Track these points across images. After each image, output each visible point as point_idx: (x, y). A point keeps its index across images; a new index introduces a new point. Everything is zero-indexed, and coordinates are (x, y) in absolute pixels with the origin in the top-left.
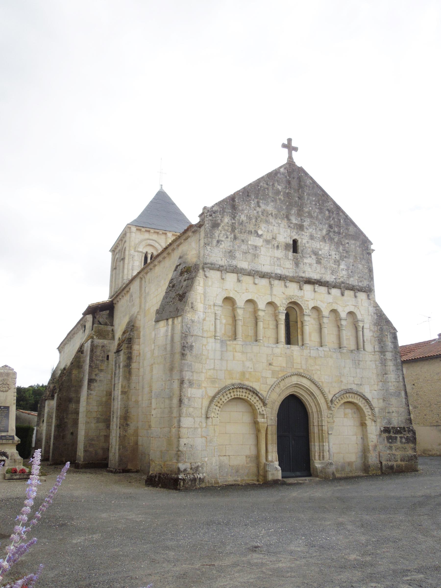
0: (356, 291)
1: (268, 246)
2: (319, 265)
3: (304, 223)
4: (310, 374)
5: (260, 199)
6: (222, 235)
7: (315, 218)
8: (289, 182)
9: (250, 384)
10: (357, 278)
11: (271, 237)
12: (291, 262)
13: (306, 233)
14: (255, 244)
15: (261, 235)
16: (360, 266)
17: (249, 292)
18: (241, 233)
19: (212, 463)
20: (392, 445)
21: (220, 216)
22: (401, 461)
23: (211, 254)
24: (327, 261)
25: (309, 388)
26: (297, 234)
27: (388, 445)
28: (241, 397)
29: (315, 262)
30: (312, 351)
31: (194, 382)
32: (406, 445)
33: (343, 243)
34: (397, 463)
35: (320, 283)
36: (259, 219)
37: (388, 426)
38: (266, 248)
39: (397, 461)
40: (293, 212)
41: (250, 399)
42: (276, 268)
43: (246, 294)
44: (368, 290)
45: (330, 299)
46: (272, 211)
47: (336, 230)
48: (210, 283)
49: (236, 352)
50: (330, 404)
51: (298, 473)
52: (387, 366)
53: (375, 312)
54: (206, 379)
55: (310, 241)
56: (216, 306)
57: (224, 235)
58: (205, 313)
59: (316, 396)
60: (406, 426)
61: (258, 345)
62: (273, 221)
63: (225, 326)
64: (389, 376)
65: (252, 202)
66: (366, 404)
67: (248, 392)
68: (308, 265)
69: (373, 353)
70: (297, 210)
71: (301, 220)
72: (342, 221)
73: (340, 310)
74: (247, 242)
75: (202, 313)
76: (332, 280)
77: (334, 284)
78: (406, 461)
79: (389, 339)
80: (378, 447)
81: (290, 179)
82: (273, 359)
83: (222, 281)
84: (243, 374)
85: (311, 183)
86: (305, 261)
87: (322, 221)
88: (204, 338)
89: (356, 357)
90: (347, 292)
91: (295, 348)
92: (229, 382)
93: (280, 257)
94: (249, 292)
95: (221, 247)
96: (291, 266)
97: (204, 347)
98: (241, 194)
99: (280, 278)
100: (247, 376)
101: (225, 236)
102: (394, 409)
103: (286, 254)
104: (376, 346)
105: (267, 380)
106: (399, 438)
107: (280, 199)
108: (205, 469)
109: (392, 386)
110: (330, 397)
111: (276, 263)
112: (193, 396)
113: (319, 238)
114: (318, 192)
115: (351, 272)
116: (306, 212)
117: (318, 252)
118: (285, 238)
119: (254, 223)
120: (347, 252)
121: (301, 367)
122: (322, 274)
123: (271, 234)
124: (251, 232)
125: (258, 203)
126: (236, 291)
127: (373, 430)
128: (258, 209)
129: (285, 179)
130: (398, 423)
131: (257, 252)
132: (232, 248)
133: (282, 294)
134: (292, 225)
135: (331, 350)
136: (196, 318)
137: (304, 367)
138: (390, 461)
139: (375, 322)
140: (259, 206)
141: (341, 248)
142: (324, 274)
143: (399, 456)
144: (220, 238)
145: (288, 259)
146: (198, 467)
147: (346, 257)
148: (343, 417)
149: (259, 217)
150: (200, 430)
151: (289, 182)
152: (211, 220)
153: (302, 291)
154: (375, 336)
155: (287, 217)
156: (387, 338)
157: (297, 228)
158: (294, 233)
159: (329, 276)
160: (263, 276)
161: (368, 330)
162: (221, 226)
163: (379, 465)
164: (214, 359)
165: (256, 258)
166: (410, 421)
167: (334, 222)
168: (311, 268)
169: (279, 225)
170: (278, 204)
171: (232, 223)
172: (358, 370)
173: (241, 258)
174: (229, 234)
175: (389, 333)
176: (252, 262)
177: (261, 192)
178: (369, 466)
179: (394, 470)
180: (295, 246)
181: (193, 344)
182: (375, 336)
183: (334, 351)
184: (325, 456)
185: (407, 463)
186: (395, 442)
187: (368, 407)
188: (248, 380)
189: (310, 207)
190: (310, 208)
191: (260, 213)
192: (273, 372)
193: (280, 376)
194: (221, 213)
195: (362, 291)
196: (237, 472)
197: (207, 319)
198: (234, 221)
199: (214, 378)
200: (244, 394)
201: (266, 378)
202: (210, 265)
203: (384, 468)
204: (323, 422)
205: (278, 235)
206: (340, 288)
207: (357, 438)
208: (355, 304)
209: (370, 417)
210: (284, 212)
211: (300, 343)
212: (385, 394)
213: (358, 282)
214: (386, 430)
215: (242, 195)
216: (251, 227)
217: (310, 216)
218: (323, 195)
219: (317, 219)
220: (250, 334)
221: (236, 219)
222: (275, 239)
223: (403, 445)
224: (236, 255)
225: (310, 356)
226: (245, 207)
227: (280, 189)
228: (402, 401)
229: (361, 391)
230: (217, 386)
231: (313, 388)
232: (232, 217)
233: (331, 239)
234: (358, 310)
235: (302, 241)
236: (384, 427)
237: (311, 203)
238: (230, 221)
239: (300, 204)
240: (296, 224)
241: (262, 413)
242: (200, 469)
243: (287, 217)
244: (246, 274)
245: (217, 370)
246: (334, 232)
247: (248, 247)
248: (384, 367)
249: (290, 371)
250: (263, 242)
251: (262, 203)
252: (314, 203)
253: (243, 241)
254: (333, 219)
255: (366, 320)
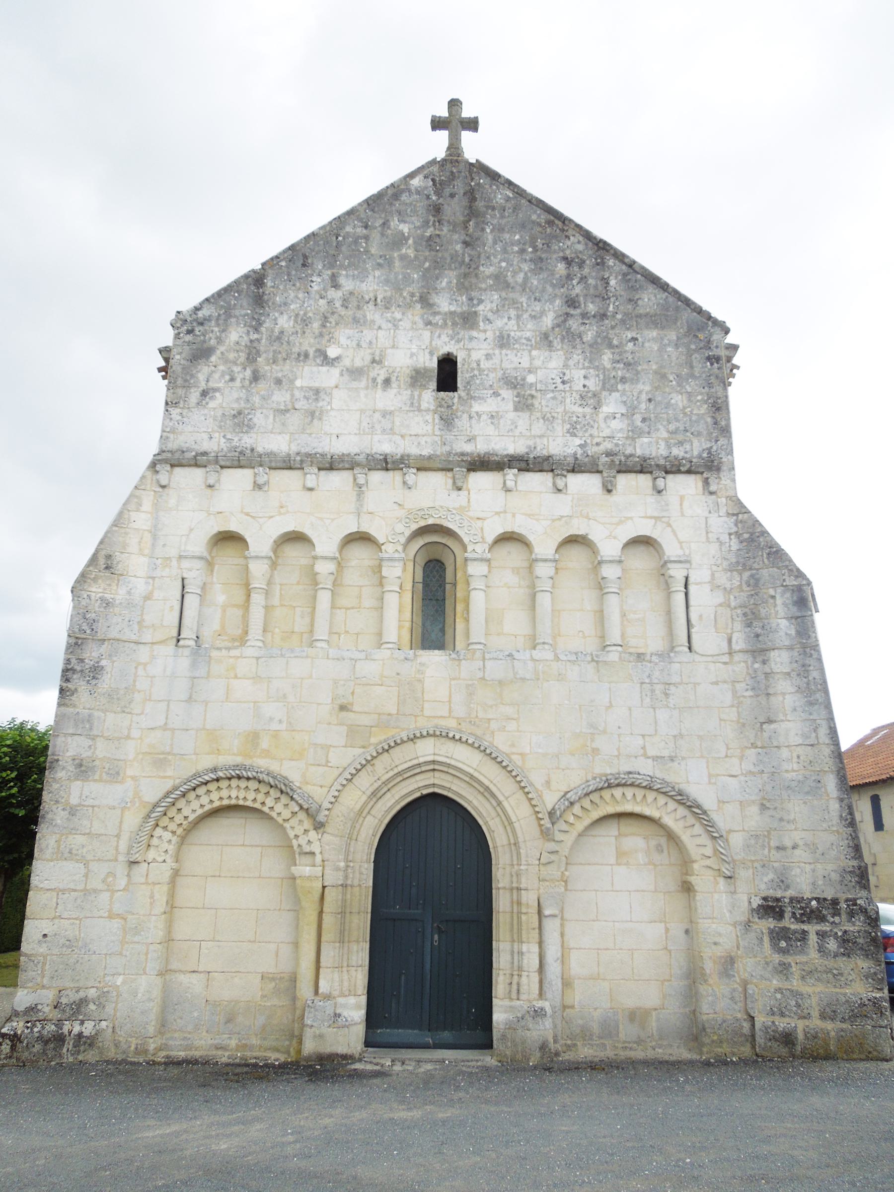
0: (657, 473)
1: (355, 384)
2: (525, 415)
3: (481, 307)
4: (479, 732)
5: (342, 267)
6: (216, 376)
7: (518, 288)
8: (437, 210)
9: (275, 767)
10: (665, 435)
11: (368, 358)
12: (429, 417)
13: (485, 331)
14: (317, 385)
15: (337, 359)
16: (678, 400)
17: (288, 512)
18: (274, 362)
19: (137, 993)
20: (789, 959)
21: (216, 329)
22: (823, 1016)
23: (180, 427)
24: (554, 398)
25: (476, 774)
26: (452, 338)
27: (777, 958)
28: (241, 803)
29: (511, 406)
30: (489, 664)
31: (97, 763)
32: (841, 962)
33: (615, 342)
34: (807, 1022)
35: (525, 464)
36: (332, 319)
37: (779, 894)
38: (348, 389)
39: (808, 1017)
40: (444, 284)
41: (272, 808)
42: (376, 438)
43: (277, 518)
44: (710, 467)
45: (562, 505)
46: (376, 291)
47: (592, 308)
48: (172, 502)
49: (236, 677)
50: (547, 823)
51: (446, 1035)
52: (775, 694)
53: (734, 529)
54: (140, 756)
55: (497, 352)
56: (186, 557)
57: (223, 376)
58: (153, 578)
59: (501, 798)
60: (842, 897)
61: (307, 657)
62: (377, 317)
63: (224, 611)
64: (781, 727)
65: (314, 279)
66: (691, 820)
67: (264, 789)
68: (484, 417)
69: (726, 658)
70: (458, 277)
71: (471, 299)
72: (613, 282)
73: (596, 534)
74: (292, 382)
75: (142, 581)
76: (570, 451)
77: (571, 460)
78: (843, 1020)
79: (780, 609)
80: (739, 965)
81: (441, 201)
82: (353, 693)
83: (209, 491)
84: (254, 737)
85: (508, 199)
86: (476, 407)
87: (544, 290)
88: (141, 646)
89: (657, 674)
90: (624, 481)
91: (434, 658)
92: (206, 762)
93: (392, 409)
94: (288, 512)
95: (212, 404)
96: (429, 428)
97: (140, 668)
98: (283, 264)
99: (386, 464)
100: (265, 743)
101: (227, 377)
102: (797, 836)
103: (412, 396)
104: (735, 637)
105: (331, 754)
106: (813, 938)
107: (403, 258)
108: (109, 1009)
109: (790, 760)
110: (550, 800)
111: (377, 427)
112: (90, 802)
113: (528, 339)
114: (534, 217)
115: (644, 420)
116: (489, 277)
117: (524, 379)
118: (412, 355)
119: (317, 332)
120: (628, 365)
121: (450, 711)
122: (534, 437)
123: (370, 351)
124: (306, 356)
125: (334, 277)
126: (247, 514)
127: (724, 911)
128: (332, 294)
129: (426, 202)
130: (814, 884)
131: (320, 404)
132: (243, 405)
133: (396, 507)
134: (438, 319)
135: (562, 657)
136: (119, 594)
137: (460, 711)
138: (782, 1015)
139: (734, 560)
140: (336, 286)
141: (607, 358)
142: (541, 436)
143: (814, 1001)
144: (211, 384)
145: (419, 410)
146: (83, 1002)
147: (623, 380)
148: (613, 860)
149: (333, 313)
150: (105, 896)
151: (437, 210)
152: (189, 343)
153: (463, 493)
154: (733, 604)
155: (425, 301)
156: (775, 606)
157: (454, 324)
158: (444, 338)
159: (560, 440)
160: (330, 464)
161: (707, 588)
162: (218, 352)
163: (746, 1025)
164: (169, 701)
165: (315, 421)
166: (862, 876)
167: (587, 287)
168: (497, 427)
169: (394, 325)
170: (397, 269)
171: (251, 341)
172: (662, 715)
173: (270, 427)
174: (236, 369)
175: (779, 590)
176: (303, 431)
177: (344, 249)
178: (704, 1029)
179: (799, 1048)
180: (447, 374)
181: (103, 663)
182: (733, 604)
183: (574, 658)
184: (524, 989)
185: (844, 1026)
186: (802, 952)
187: (698, 829)
188: (267, 754)
189: (501, 261)
190: (504, 264)
191: (338, 304)
192: (353, 731)
193: (373, 740)
194: (221, 322)
195: (679, 472)
196: (229, 1021)
197: (156, 594)
198: (256, 336)
199: (163, 753)
200: (251, 795)
201: (327, 748)
202: (169, 455)
203: (760, 1040)
204: (523, 880)
205: (389, 351)
206: (598, 472)
207: (667, 930)
208: (656, 514)
209: (708, 862)
210: (415, 288)
211: (460, 645)
212: (768, 788)
213: (669, 446)
214: (771, 908)
215: (287, 267)
216: (308, 344)
217: (500, 282)
218: (550, 223)
219: (524, 290)
220: (296, 629)
221: (263, 329)
222: (379, 362)
223: (830, 963)
224: (255, 420)
225: (483, 679)
226: (292, 295)
227: (406, 230)
228: (827, 809)
229: (671, 778)
230: (169, 773)
231: (490, 774)
232: (251, 326)
233: (572, 338)
234: (669, 529)
235: (469, 356)
236: (765, 899)
237: (505, 251)
238: (246, 338)
239: (467, 260)
240: (452, 313)
241: (307, 849)
242: (92, 1007)
243: (425, 301)
244: (279, 465)
245: (173, 730)
246: (584, 315)
247: (292, 395)
248: (763, 699)
249: (410, 726)
250: (342, 375)
251: (347, 276)
252: (516, 249)
253: (279, 382)
254: (583, 279)
255: (696, 559)
